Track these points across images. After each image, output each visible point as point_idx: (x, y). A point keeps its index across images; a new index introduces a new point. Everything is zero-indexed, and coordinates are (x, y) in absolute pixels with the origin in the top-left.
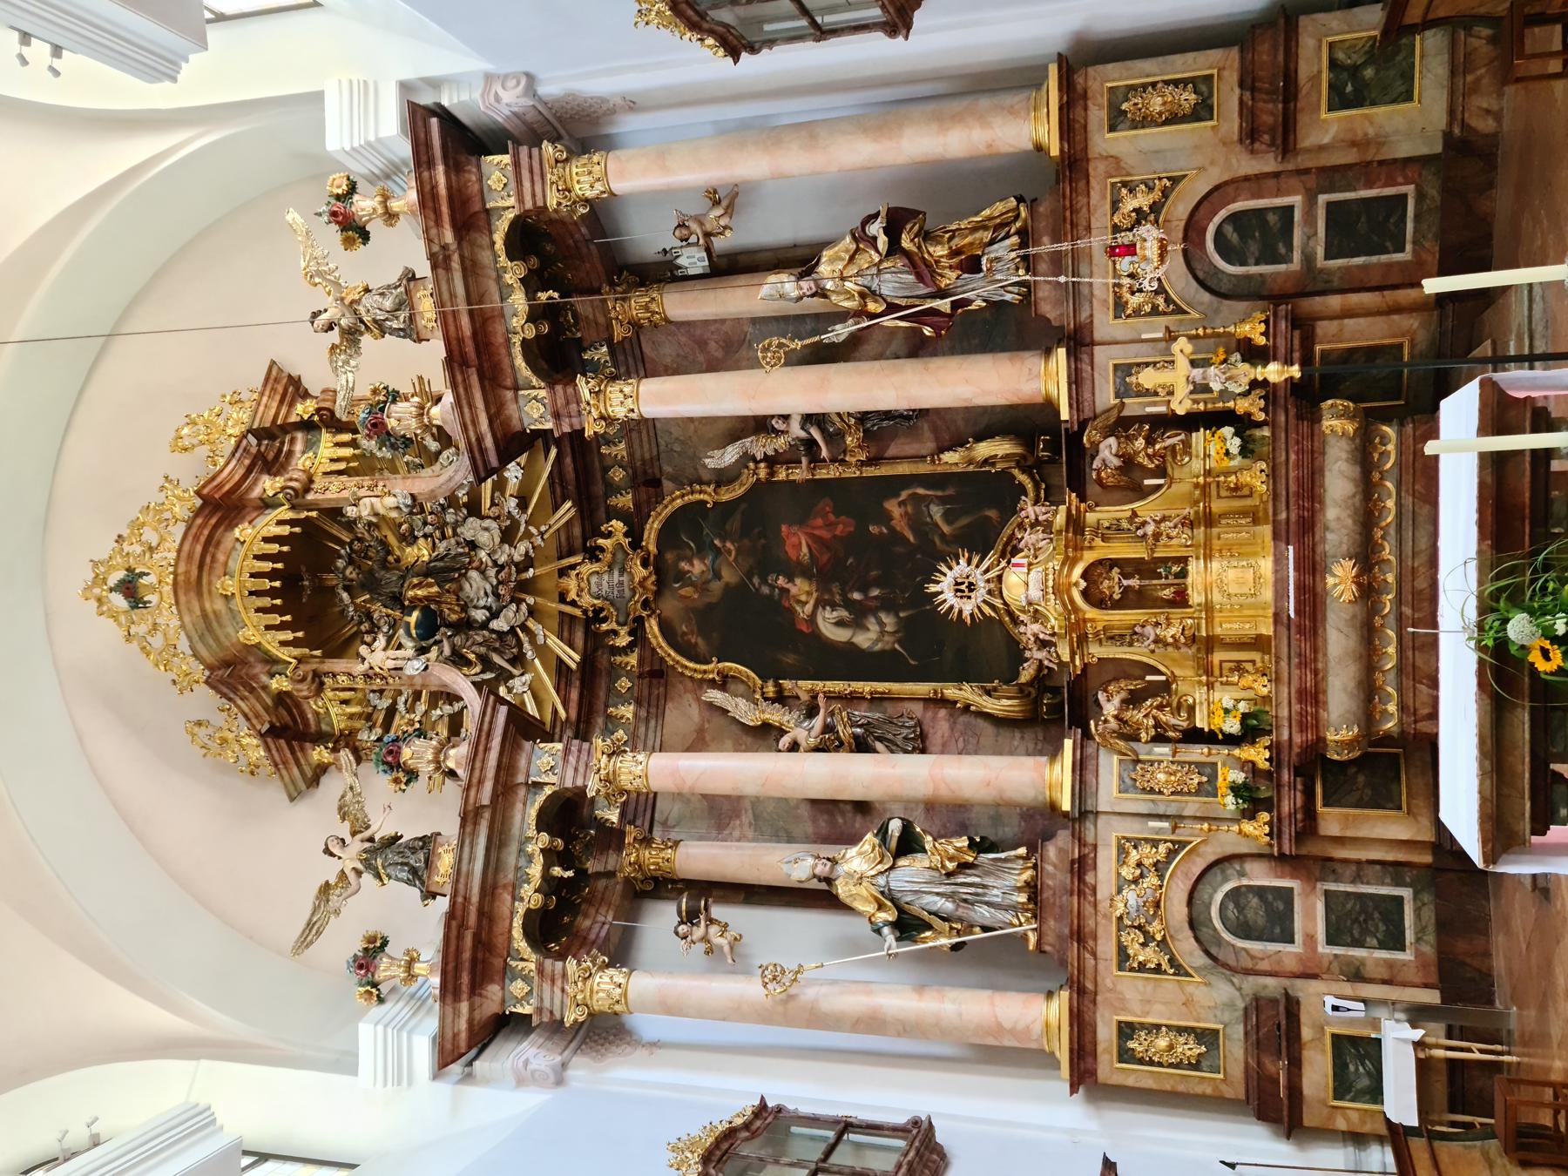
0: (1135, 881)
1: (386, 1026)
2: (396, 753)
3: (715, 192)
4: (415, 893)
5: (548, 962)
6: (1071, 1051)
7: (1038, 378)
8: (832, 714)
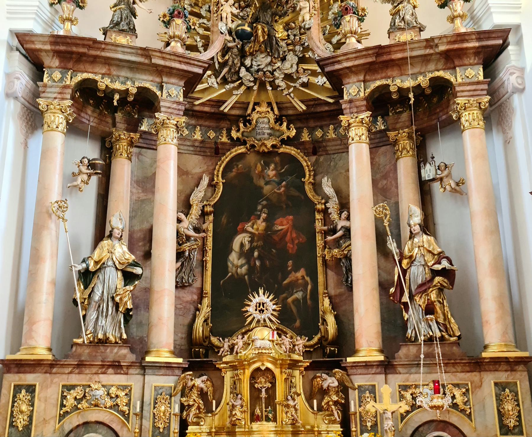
0: (108, 394)
1: (38, 7)
2: (179, 16)
3: (463, 184)
4: (106, 24)
5: (70, 91)
6: (21, 360)
7: (368, 343)
8: (196, 240)
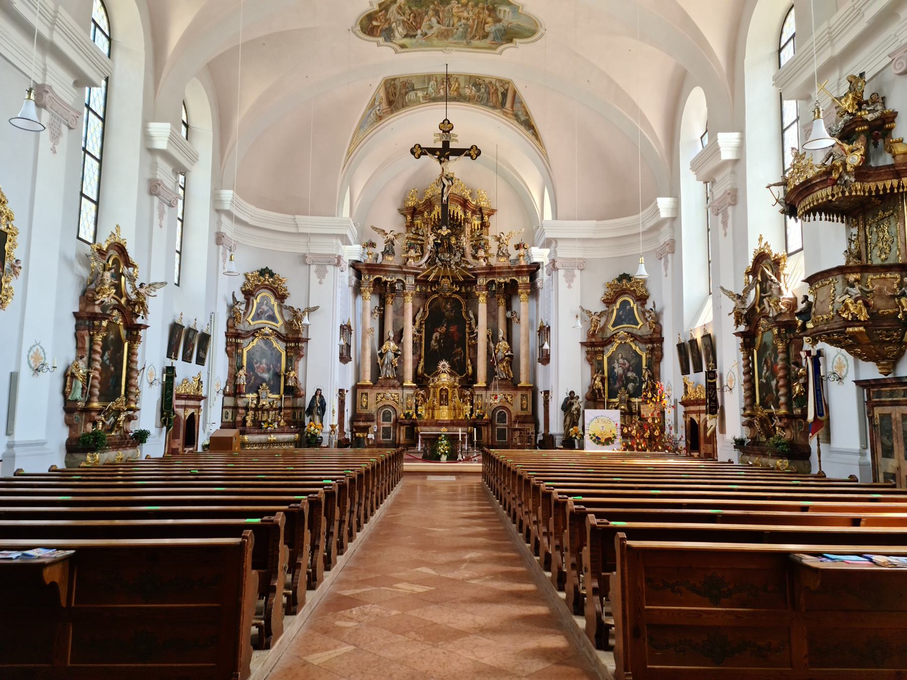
7: (481, 383)
